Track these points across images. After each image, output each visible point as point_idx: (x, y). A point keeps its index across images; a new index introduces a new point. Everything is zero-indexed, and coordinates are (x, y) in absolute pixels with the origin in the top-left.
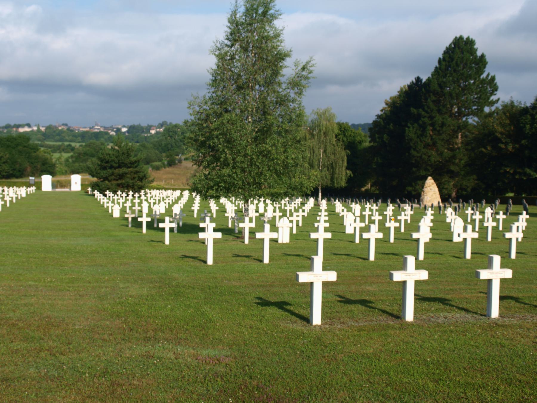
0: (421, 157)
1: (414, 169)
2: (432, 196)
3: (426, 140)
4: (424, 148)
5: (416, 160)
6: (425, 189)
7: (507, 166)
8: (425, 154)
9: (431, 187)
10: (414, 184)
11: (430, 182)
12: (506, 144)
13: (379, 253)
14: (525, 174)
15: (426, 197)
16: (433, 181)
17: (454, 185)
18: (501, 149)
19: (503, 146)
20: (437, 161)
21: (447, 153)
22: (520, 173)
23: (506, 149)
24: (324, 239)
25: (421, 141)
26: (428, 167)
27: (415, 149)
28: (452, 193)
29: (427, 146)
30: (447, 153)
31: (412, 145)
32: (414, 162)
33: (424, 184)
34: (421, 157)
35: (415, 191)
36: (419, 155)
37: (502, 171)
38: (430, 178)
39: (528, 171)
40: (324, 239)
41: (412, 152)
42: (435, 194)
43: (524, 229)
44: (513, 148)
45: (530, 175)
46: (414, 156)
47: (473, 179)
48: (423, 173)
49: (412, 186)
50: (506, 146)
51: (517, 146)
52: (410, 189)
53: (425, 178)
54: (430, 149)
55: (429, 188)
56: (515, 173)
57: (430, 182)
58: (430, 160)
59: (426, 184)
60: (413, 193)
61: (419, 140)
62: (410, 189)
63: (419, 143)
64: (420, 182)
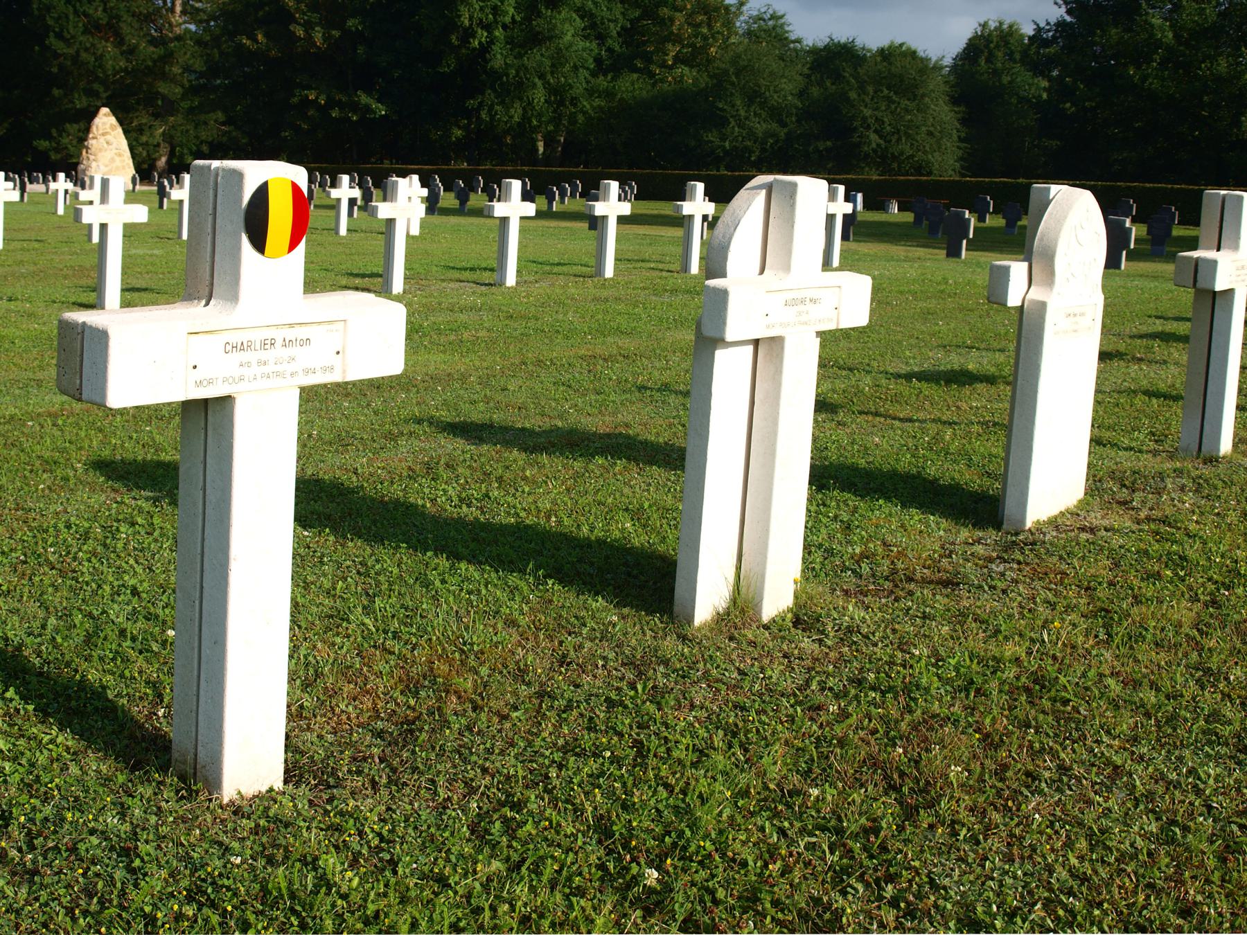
0: (75, 58)
1: (56, 92)
2: (112, 160)
3: (91, 12)
4: (83, 33)
5: (61, 67)
6: (92, 143)
7: (309, 88)
8: (87, 50)
9: (108, 137)
10: (54, 132)
11: (105, 121)
12: (308, 26)
13: (1197, 265)
14: (355, 107)
15: (94, 164)
16: (113, 120)
17: (163, 134)
18: (293, 37)
19: (300, 32)
20: (122, 70)
21: (148, 51)
22: (340, 104)
23: (309, 38)
24: (312, 398)
25: (76, 12)
26: (96, 86)
27: (59, 36)
28: (159, 159)
29: (94, 28)
30: (148, 51)
31: (50, 22)
32: (55, 70)
33: (88, 130)
34: (75, 58)
35: (57, 150)
36: (71, 51)
37: (295, 100)
38: (105, 110)
39: (364, 99)
40: (312, 398)
41: (52, 40)
42: (120, 155)
43: (415, 231)
44: (326, 38)
45: (368, 109)
46: (56, 55)
47: (216, 121)
48: (81, 102)
49: (49, 137)
50: (306, 31)
51: (336, 33)
52: (43, 144)
53: (94, 114)
54: (101, 38)
55: (102, 140)
56: (331, 103)
57: (105, 121)
58: (100, 66)
59: (94, 129)
60: (54, 156)
61: (71, 9)
62: (43, 144)
63: (71, 17)
64: (72, 128)
